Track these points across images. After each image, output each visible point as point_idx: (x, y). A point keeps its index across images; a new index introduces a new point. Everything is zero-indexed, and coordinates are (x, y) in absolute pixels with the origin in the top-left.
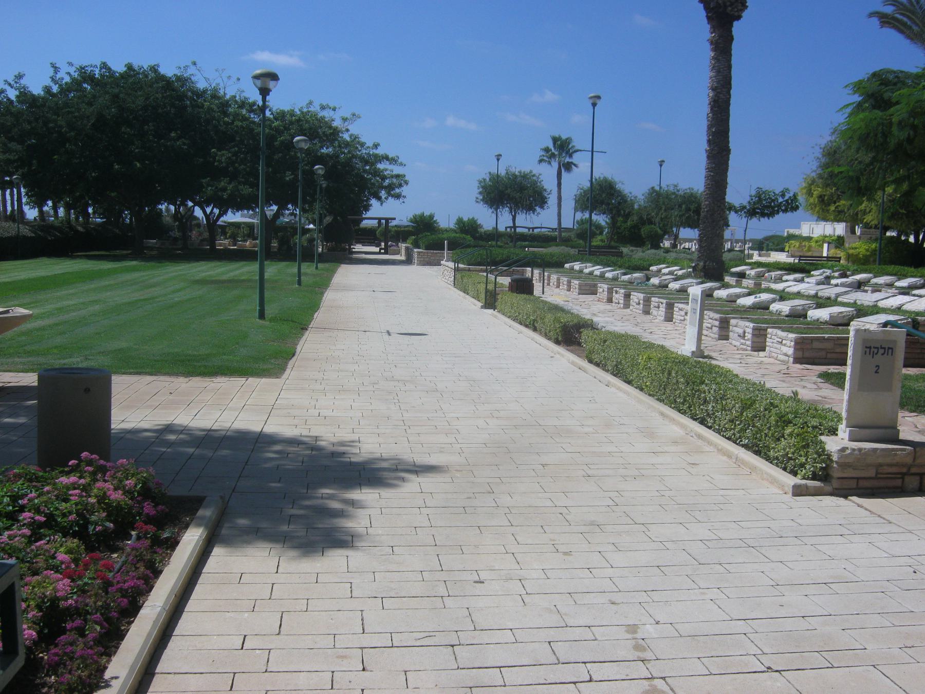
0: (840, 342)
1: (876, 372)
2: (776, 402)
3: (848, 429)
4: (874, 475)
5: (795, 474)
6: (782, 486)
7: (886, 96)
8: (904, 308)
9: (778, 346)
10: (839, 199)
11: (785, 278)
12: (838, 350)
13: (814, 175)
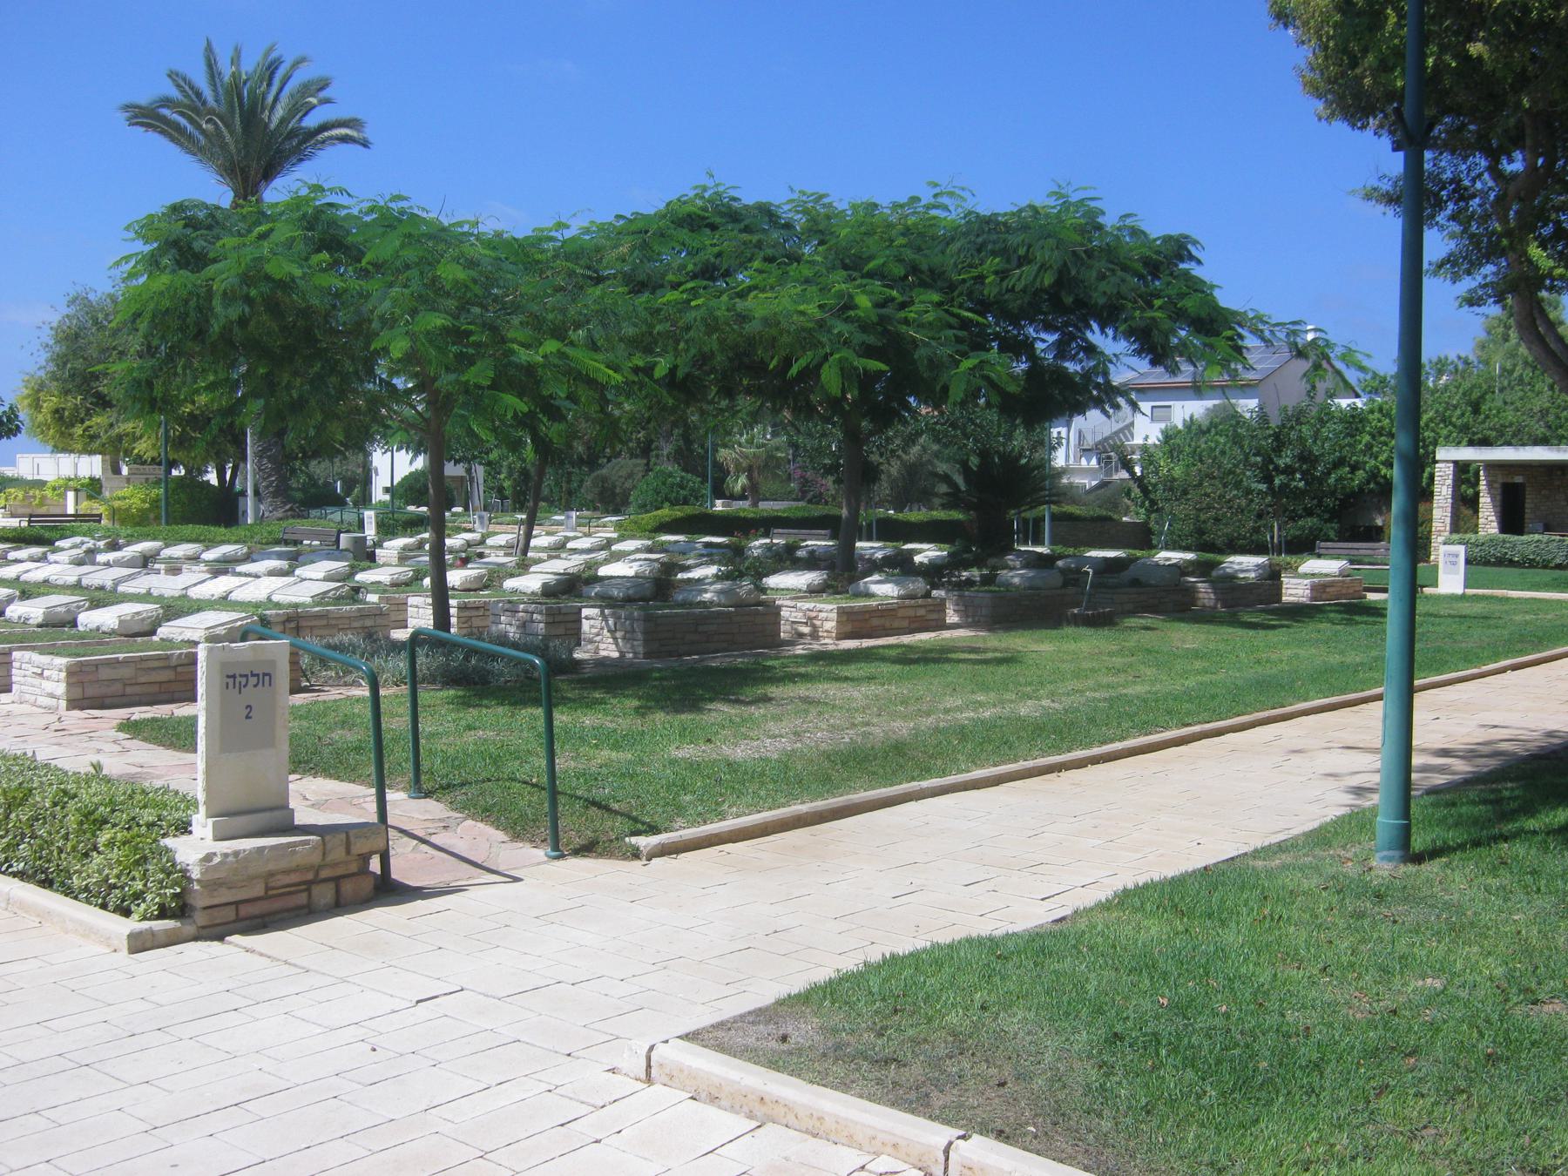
0: (145, 665)
1: (248, 717)
2: (71, 787)
3: (210, 821)
4: (262, 893)
5: (127, 913)
6: (106, 940)
7: (198, 245)
8: (233, 597)
9: (37, 681)
10: (89, 414)
11: (12, 555)
12: (143, 680)
13: (42, 373)
